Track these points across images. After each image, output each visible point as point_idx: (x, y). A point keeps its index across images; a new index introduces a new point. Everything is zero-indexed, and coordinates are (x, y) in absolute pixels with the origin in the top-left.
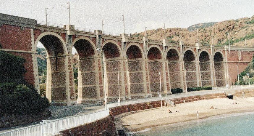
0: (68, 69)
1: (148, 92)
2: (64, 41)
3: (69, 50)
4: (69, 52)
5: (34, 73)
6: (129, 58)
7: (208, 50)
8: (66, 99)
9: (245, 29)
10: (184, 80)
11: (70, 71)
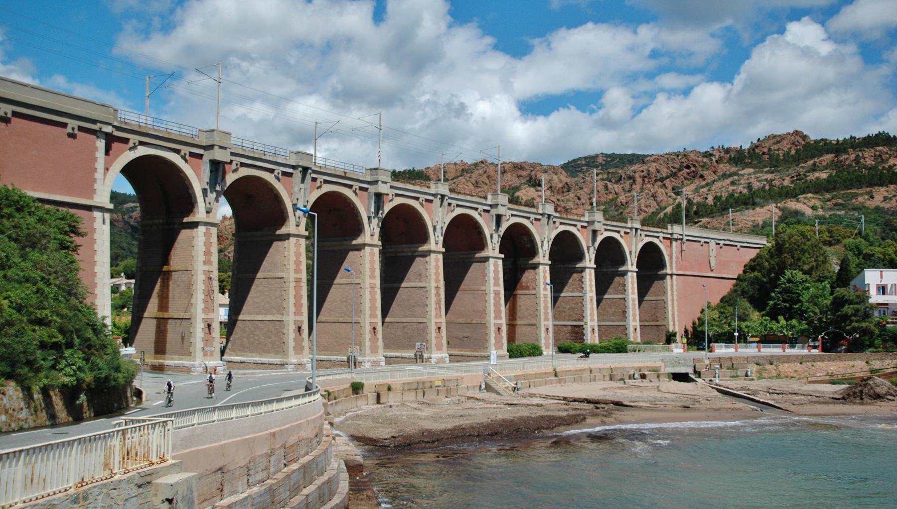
0: (202, 263)
1: (439, 348)
2: (195, 178)
3: (208, 206)
4: (208, 212)
5: (97, 269)
6: (127, 408)
7: (622, 233)
8: (190, 354)
9: (730, 179)
10: (546, 319)
11: (206, 268)
